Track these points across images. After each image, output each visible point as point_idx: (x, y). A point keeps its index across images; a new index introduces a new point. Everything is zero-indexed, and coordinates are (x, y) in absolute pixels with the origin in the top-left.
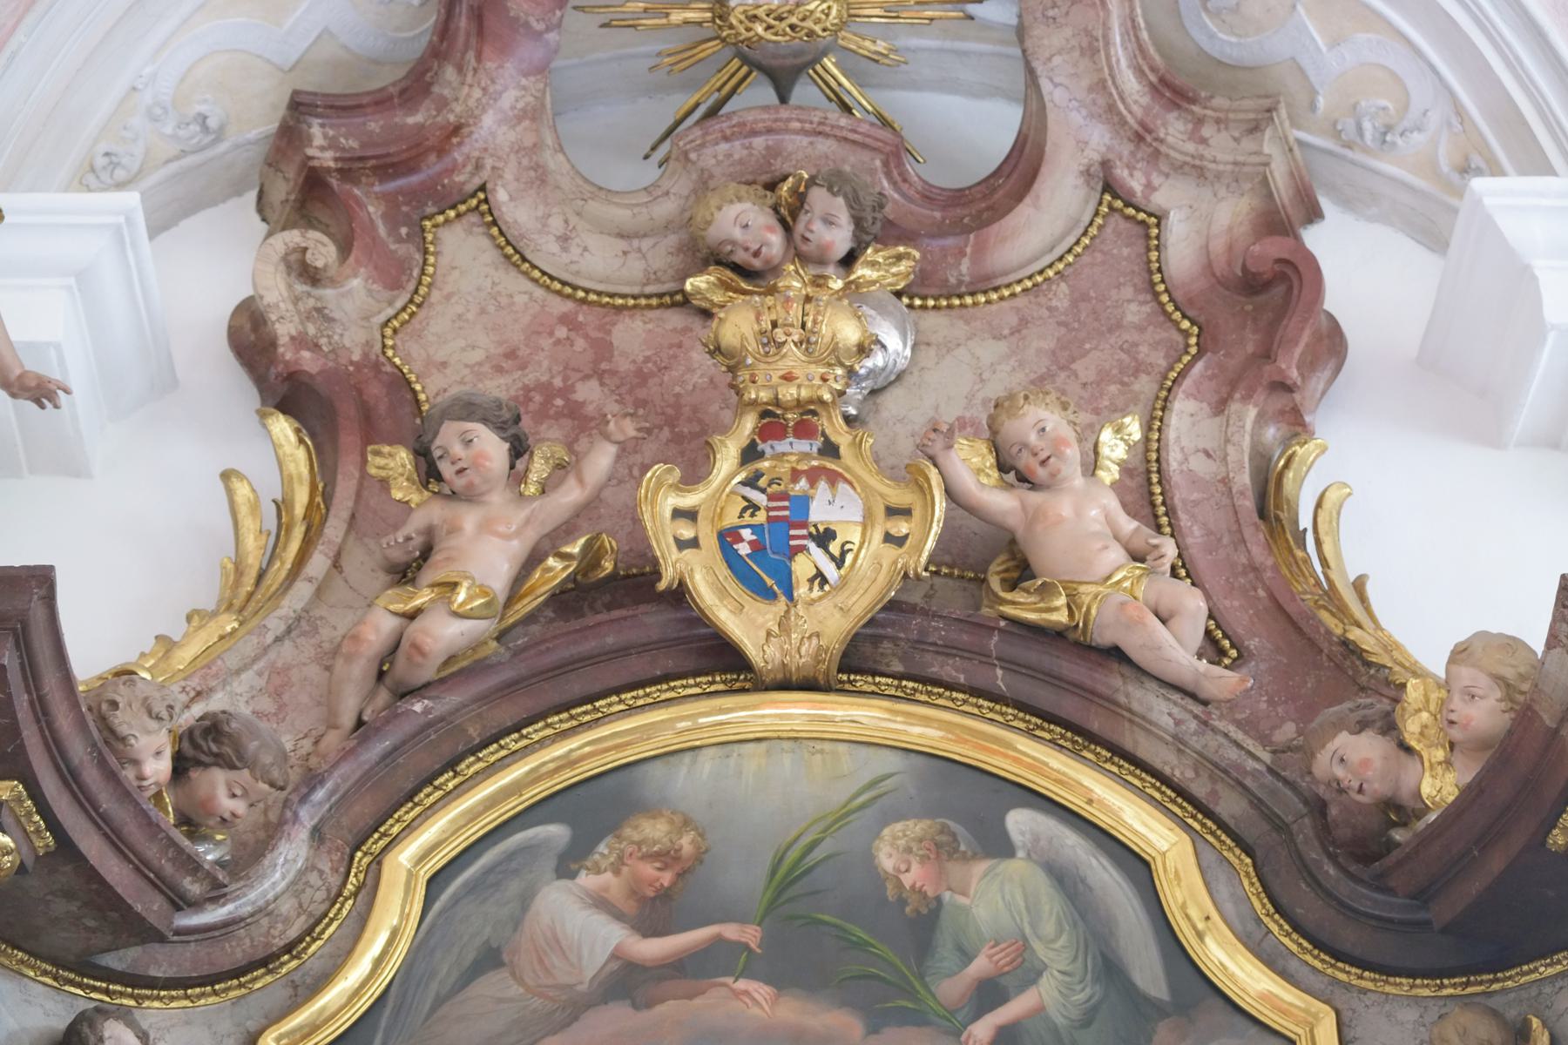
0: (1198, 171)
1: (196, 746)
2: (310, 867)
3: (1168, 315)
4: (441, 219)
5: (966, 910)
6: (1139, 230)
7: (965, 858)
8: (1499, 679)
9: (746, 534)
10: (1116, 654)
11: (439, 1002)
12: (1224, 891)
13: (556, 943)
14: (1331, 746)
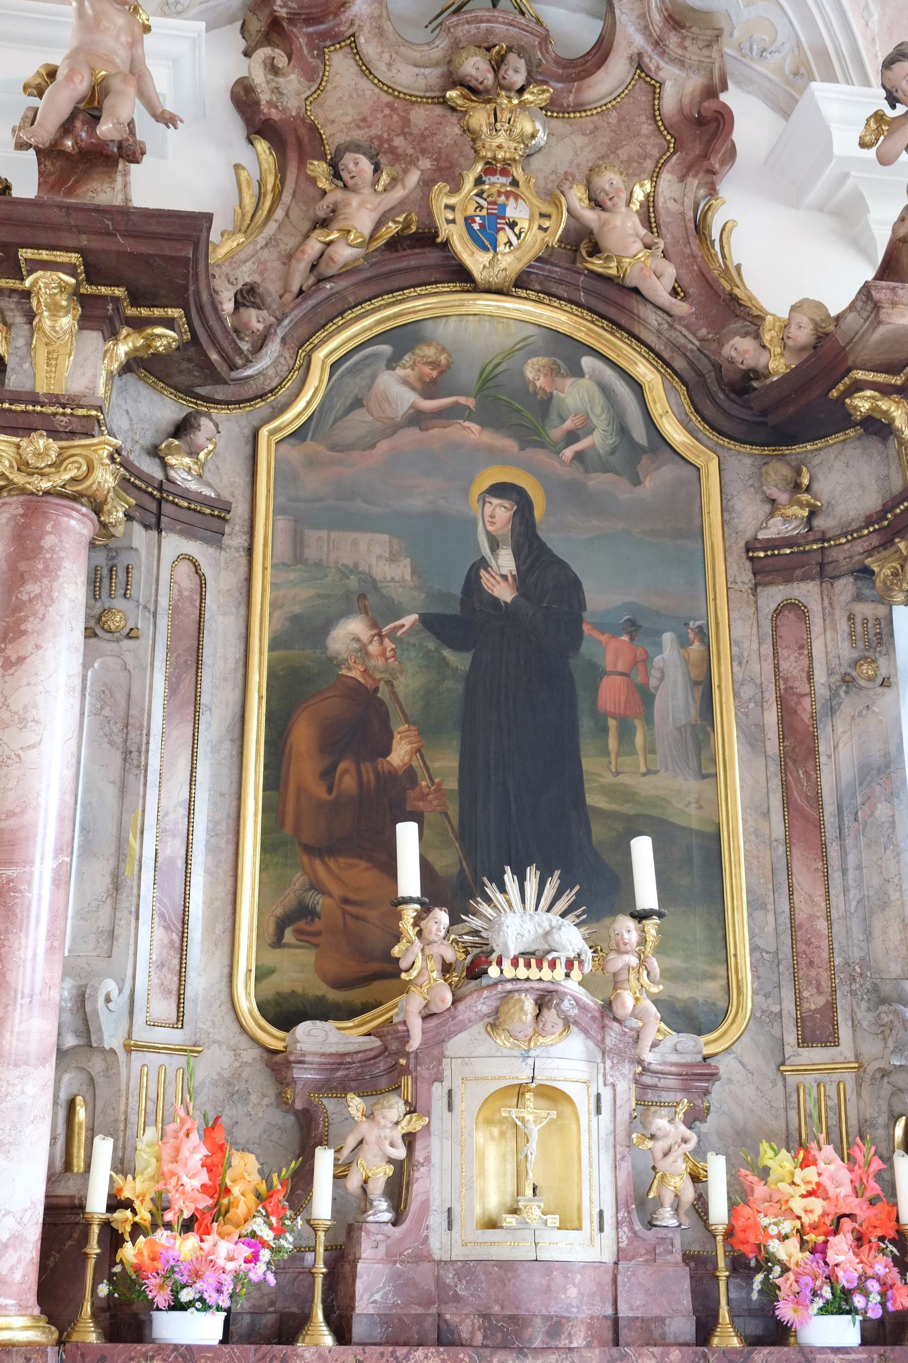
0: (681, 63)
1: (244, 298)
2: (281, 355)
3: (661, 132)
4: (332, 48)
5: (563, 399)
6: (650, 89)
7: (563, 376)
8: (813, 321)
9: (478, 219)
10: (636, 291)
11: (336, 420)
12: (673, 402)
13: (386, 398)
14: (731, 343)
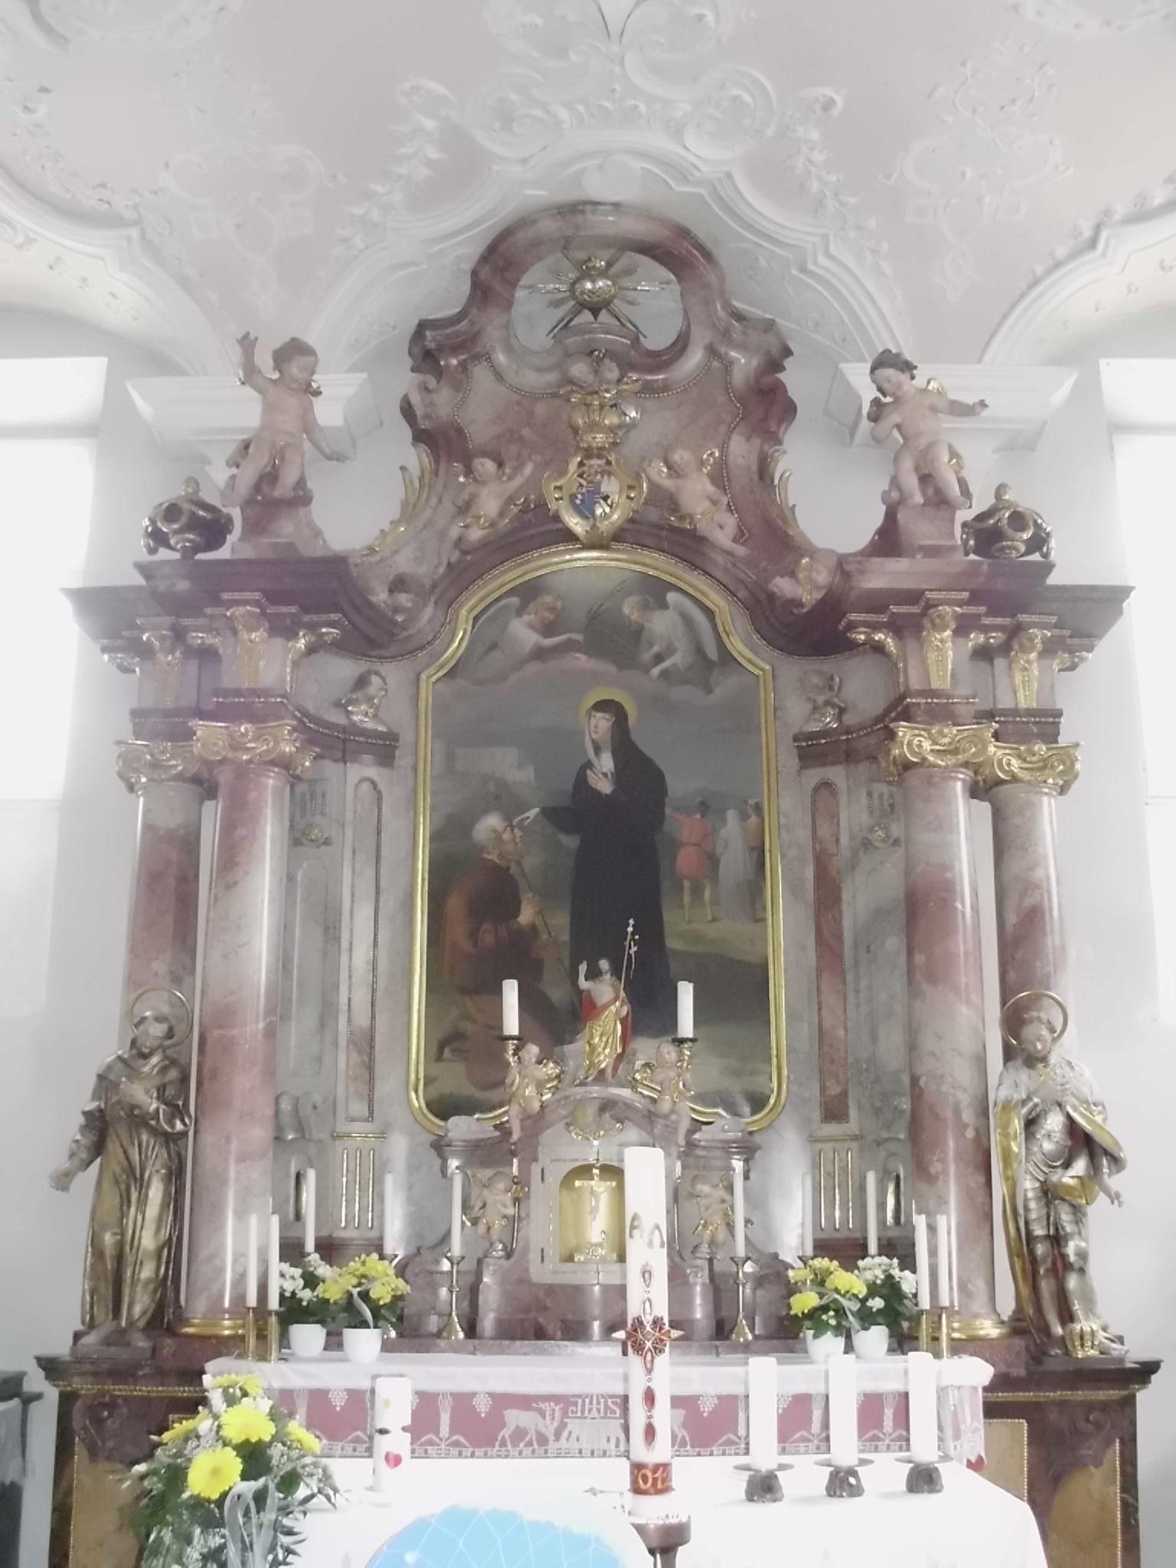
9: (579, 496)
